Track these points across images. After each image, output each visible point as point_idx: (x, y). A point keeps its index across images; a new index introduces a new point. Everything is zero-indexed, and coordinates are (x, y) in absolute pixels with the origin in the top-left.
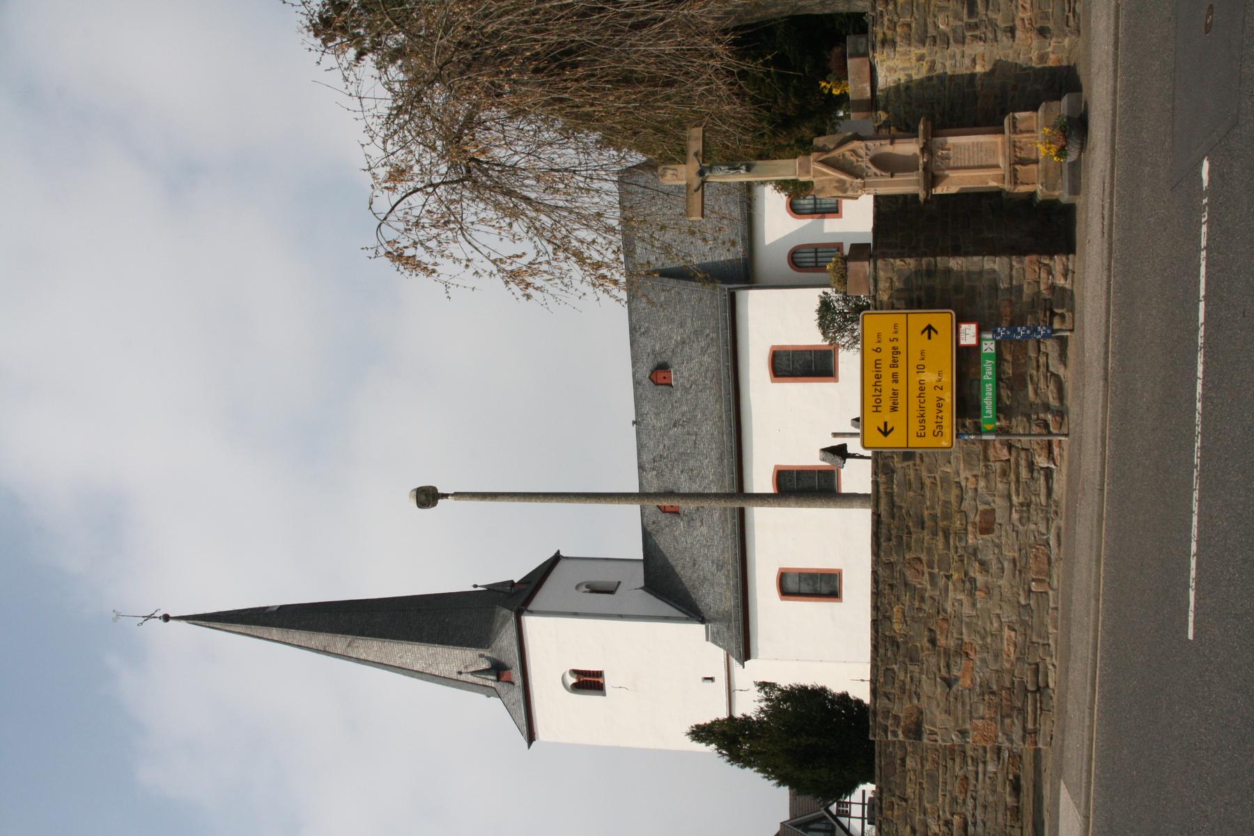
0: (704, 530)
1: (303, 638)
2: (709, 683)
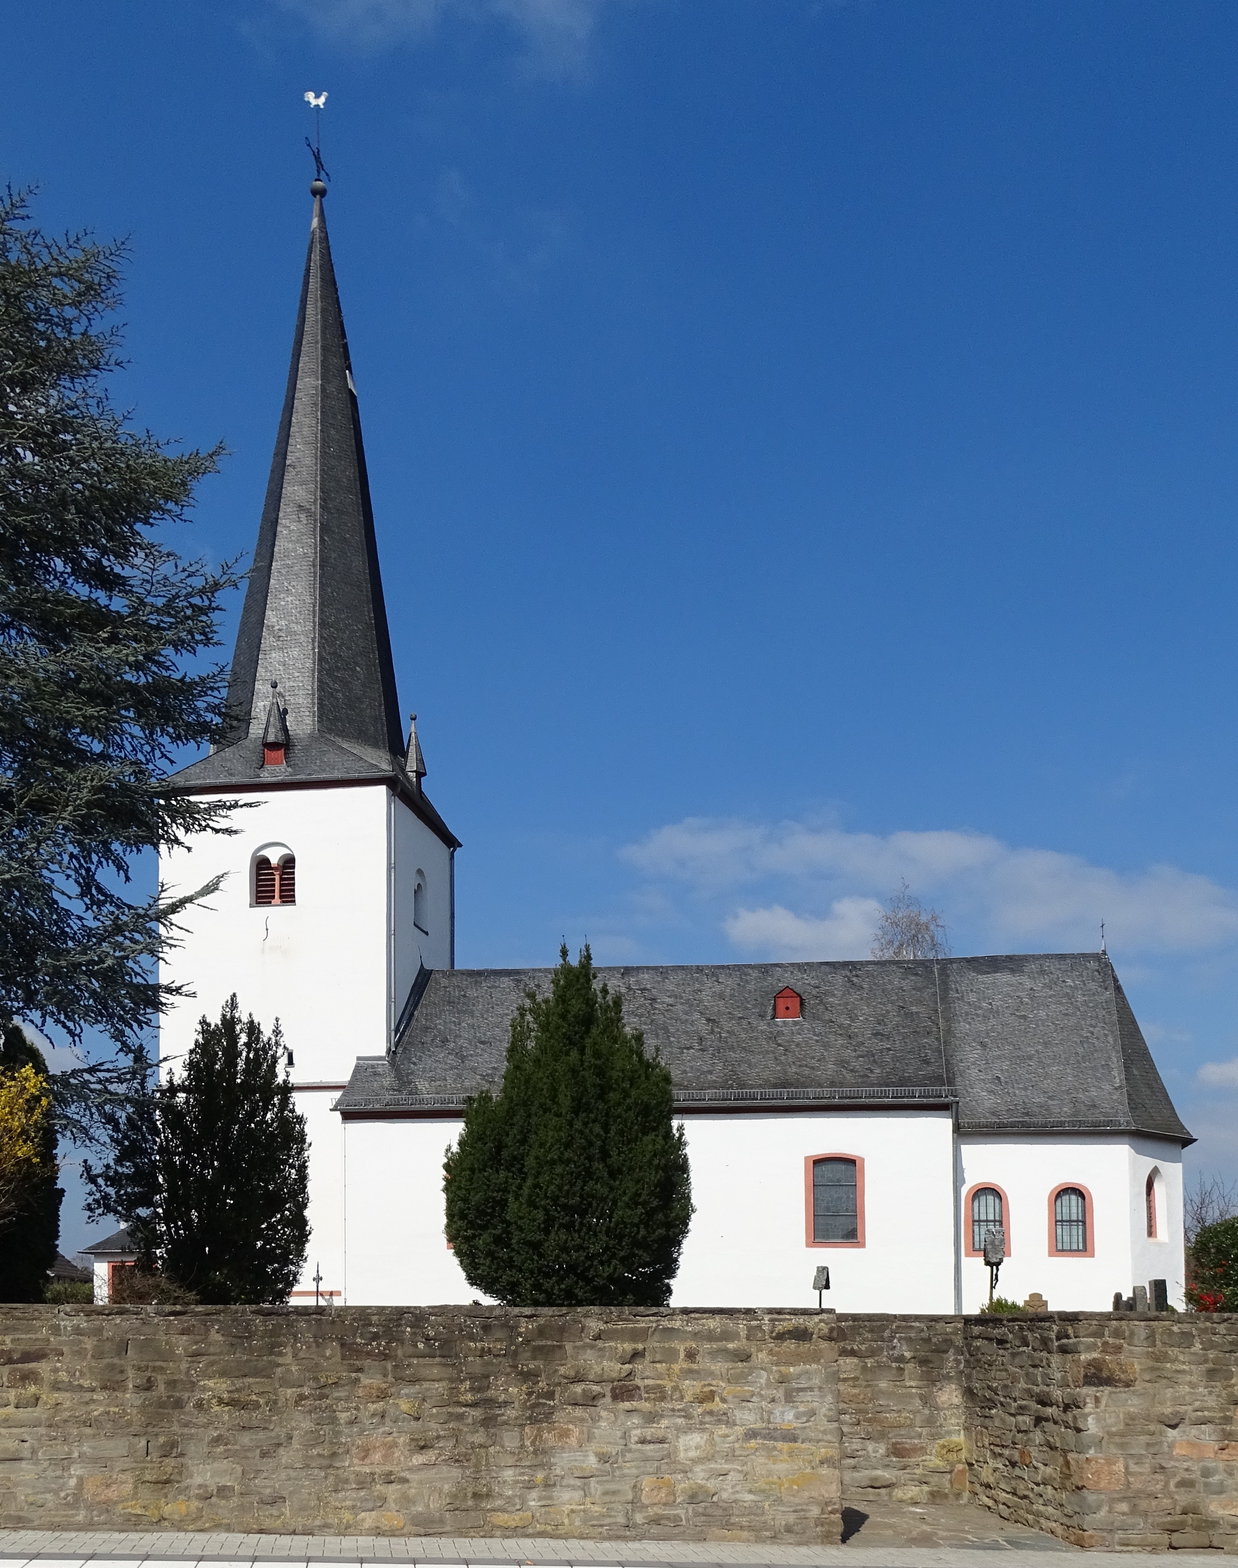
1: (306, 431)
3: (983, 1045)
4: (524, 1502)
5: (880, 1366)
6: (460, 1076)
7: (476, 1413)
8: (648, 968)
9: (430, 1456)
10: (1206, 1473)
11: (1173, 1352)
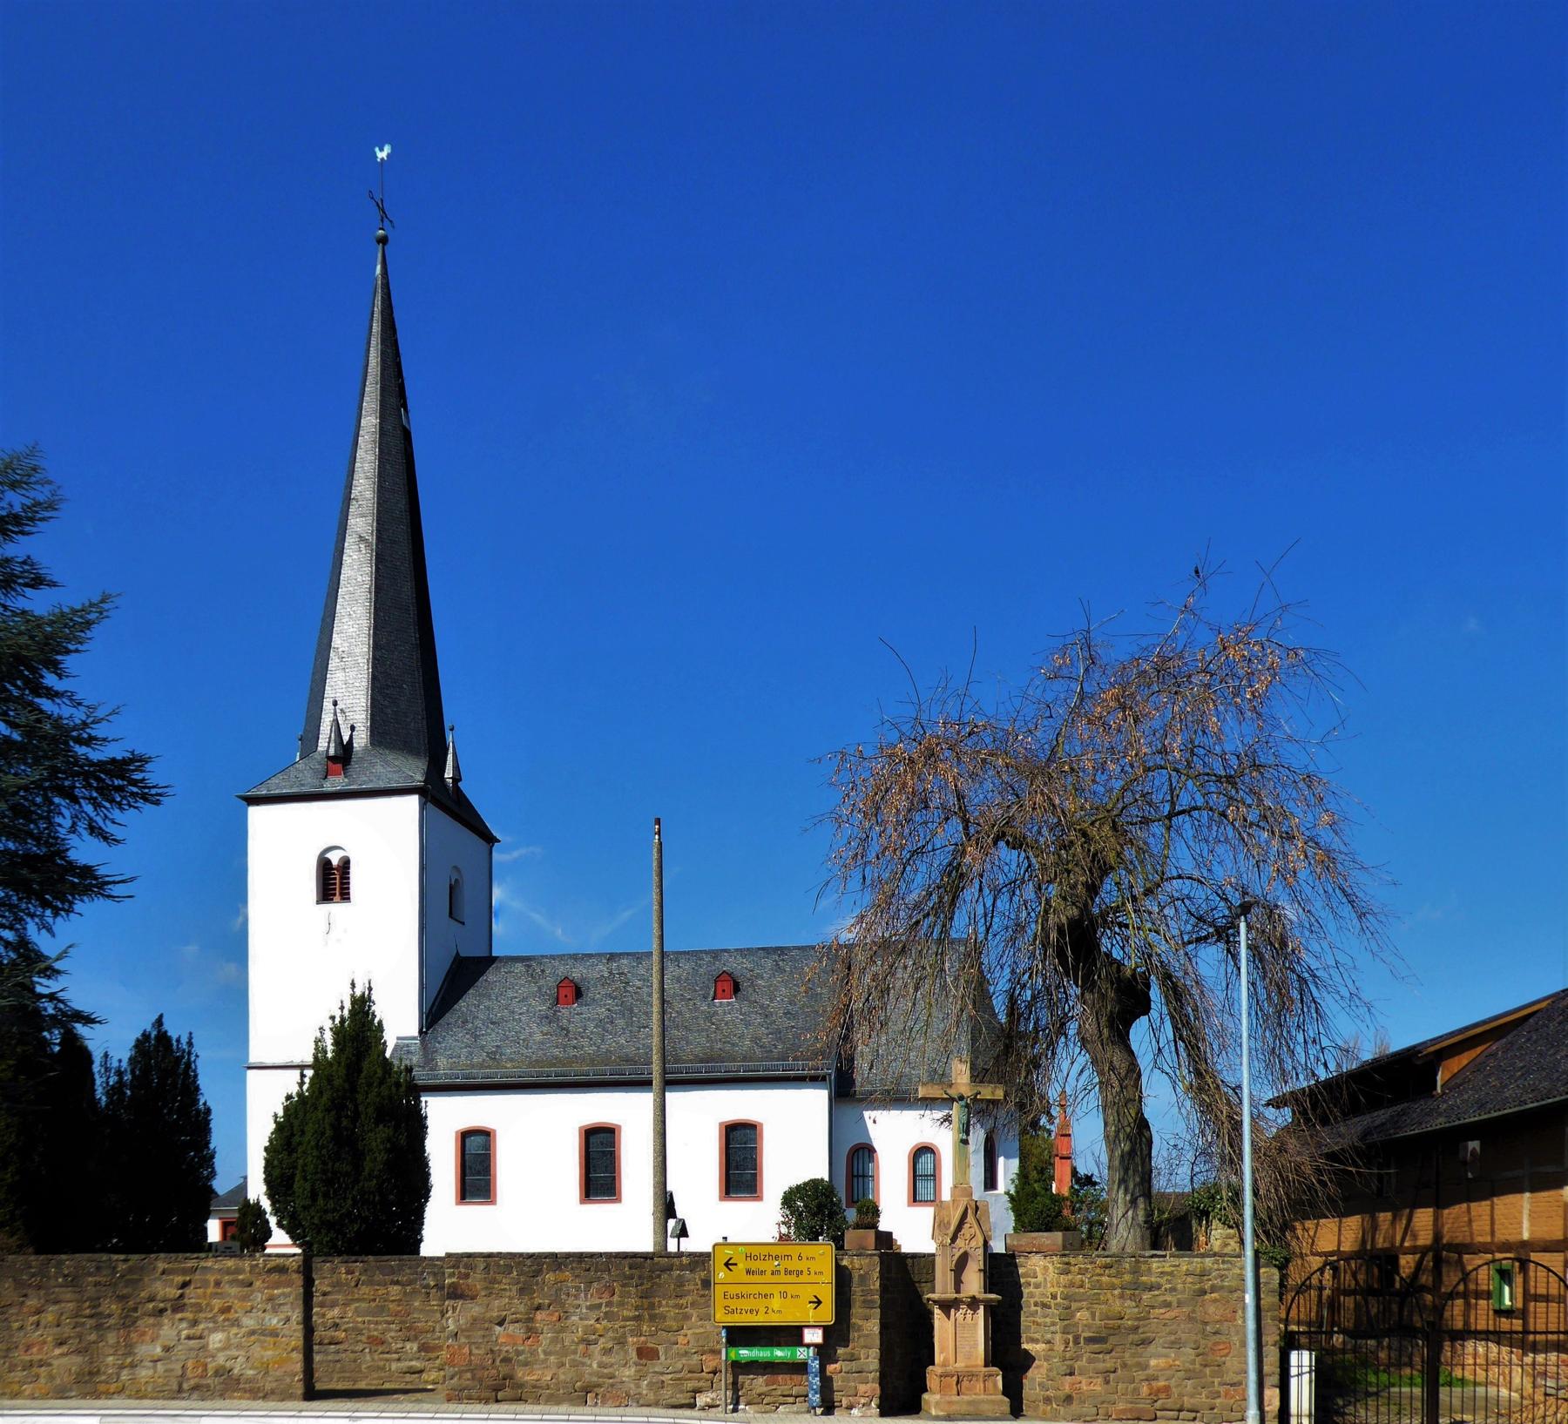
0: (538, 1037)
4: (118, 1375)
5: (414, 1292)
6: (471, 1053)
7: (91, 1322)
9: (64, 1349)
10: (518, 1353)
11: (499, 1277)
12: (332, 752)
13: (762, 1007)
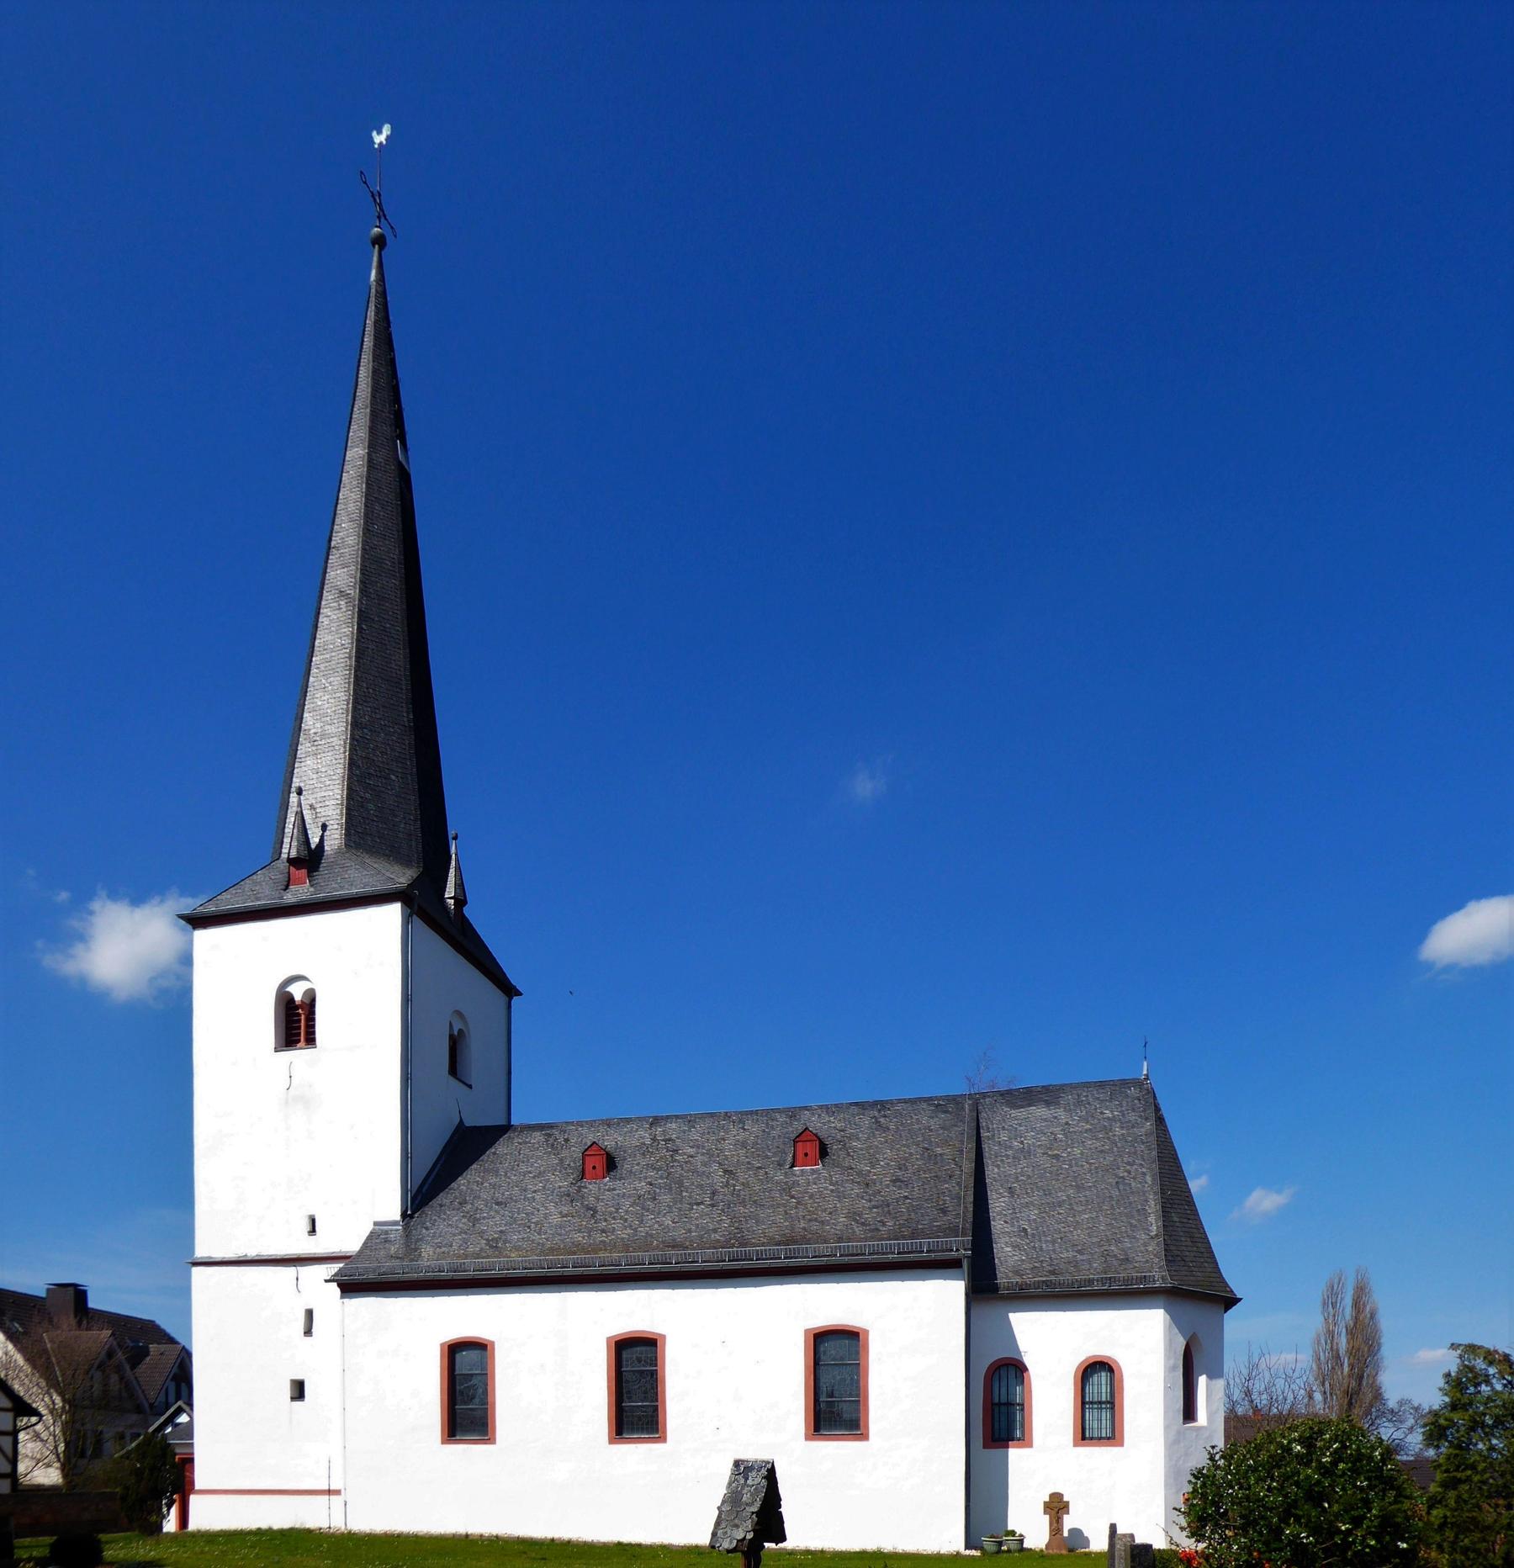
0: (556, 1219)
1: (352, 507)
2: (306, 1227)
3: (1011, 1191)
8: (677, 1117)
12: (294, 854)
13: (860, 1173)
